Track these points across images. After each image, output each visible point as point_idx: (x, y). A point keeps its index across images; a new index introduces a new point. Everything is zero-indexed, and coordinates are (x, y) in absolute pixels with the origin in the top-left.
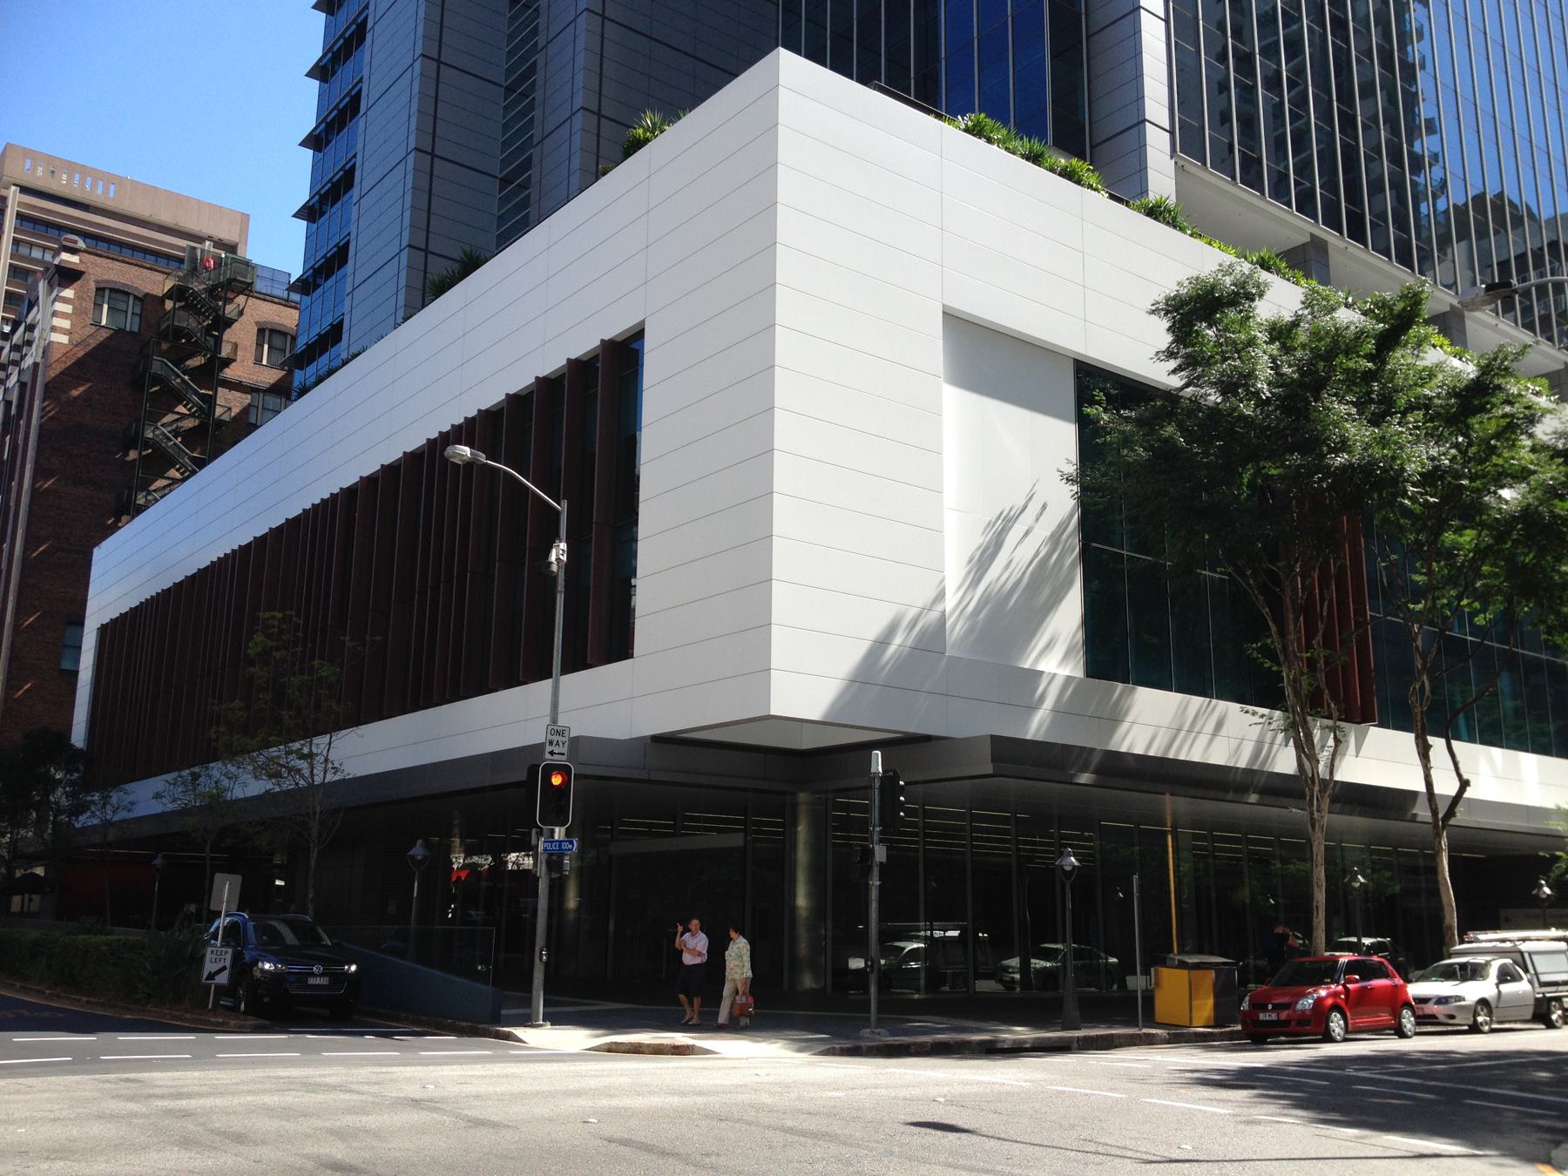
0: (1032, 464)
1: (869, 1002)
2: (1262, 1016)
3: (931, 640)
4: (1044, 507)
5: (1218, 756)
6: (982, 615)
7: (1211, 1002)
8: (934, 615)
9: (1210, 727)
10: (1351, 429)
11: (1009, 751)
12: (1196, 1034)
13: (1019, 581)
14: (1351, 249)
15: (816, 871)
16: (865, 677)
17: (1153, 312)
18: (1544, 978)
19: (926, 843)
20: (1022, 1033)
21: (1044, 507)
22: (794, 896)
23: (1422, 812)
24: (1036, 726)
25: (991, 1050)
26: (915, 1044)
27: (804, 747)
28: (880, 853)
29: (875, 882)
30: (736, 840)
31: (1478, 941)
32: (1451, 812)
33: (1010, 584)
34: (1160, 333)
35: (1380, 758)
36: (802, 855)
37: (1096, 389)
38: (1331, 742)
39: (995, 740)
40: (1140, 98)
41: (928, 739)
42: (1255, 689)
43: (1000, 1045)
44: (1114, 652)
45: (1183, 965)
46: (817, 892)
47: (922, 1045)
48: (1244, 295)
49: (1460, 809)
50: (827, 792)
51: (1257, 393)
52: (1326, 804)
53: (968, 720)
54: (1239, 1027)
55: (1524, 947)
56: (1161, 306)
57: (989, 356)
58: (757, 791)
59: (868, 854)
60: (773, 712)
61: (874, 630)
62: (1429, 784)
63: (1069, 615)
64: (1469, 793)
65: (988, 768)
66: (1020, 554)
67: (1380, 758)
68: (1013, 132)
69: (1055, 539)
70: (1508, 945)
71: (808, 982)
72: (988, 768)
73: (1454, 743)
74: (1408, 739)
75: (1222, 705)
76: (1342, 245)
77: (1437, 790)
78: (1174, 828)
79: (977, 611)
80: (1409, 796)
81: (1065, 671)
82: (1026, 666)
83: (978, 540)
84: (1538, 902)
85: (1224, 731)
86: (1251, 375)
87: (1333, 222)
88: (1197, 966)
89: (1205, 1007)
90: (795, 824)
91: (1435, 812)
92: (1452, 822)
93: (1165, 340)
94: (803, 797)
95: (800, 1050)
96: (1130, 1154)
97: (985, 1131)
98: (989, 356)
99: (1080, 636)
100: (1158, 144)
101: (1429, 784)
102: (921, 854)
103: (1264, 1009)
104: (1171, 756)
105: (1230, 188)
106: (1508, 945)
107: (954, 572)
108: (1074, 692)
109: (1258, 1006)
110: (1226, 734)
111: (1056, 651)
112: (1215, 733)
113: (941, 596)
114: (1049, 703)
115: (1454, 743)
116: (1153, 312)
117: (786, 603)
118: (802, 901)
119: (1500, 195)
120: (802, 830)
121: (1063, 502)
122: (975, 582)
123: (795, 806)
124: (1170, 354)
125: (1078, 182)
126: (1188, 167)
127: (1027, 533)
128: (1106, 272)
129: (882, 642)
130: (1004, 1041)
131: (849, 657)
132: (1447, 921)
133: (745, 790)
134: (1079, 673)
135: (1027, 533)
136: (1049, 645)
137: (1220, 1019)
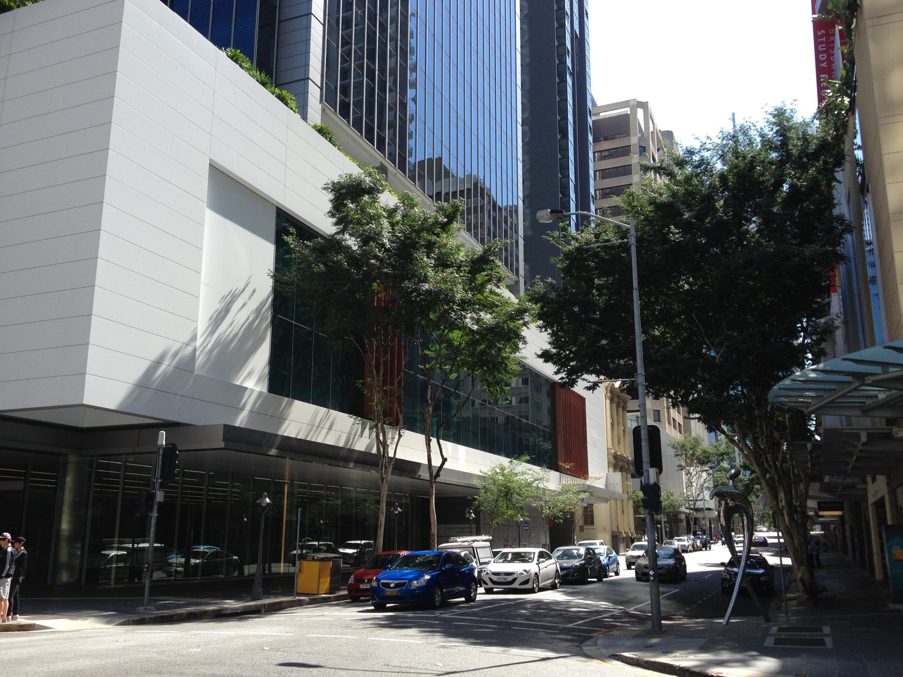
0: (248, 266)
1: (144, 587)
2: (362, 586)
3: (185, 366)
4: (254, 291)
5: (330, 441)
6: (215, 352)
7: (329, 579)
8: (189, 349)
9: (327, 426)
10: (431, 273)
11: (232, 434)
12: (322, 598)
13: (236, 334)
14: (398, 175)
15: (78, 505)
16: (143, 385)
17: (325, 189)
18: (482, 561)
19: (125, 489)
20: (231, 604)
21: (254, 291)
22: (60, 522)
23: (424, 474)
24: (241, 421)
25: (220, 616)
26: (177, 615)
27: (85, 426)
28: (160, 496)
29: (155, 514)
30: (19, 485)
31: (457, 541)
32: (438, 475)
33: (232, 335)
34: (325, 201)
35: (410, 447)
36: (68, 497)
37: (286, 227)
38: (397, 437)
39: (225, 426)
40: (307, 65)
41: (191, 425)
42: (354, 405)
43: (224, 612)
44: (285, 380)
45: (314, 559)
46: (78, 522)
47: (180, 615)
48: (372, 191)
49: (442, 473)
50: (92, 456)
51: (383, 245)
52: (390, 470)
53: (207, 416)
54: (346, 592)
55: (475, 544)
56: (330, 186)
57: (232, 195)
58: (35, 452)
59: (152, 496)
60: (86, 401)
61: (154, 355)
62: (429, 460)
63: (261, 357)
64: (447, 466)
65: (222, 445)
66: (239, 317)
67: (410, 447)
68: (255, 65)
69: (258, 311)
70: (466, 544)
71: (65, 577)
72: (222, 445)
73: (441, 441)
74: (421, 438)
75: (335, 414)
76: (395, 171)
77: (433, 464)
78: (292, 480)
79: (212, 350)
80: (416, 466)
81: (258, 389)
82: (238, 384)
83: (216, 306)
84: (468, 521)
85: (334, 428)
86: (379, 234)
87: (392, 158)
88: (322, 560)
89: (326, 583)
90: (64, 476)
91: (431, 474)
92: (438, 480)
93: (329, 206)
94: (72, 458)
95: (108, 623)
96: (412, 670)
97: (330, 663)
98: (232, 195)
99: (267, 370)
100: (314, 93)
101: (429, 460)
102: (120, 494)
103: (363, 582)
104: (308, 439)
105: (346, 128)
106: (466, 544)
107: (202, 325)
108: (263, 401)
109: (360, 580)
110: (336, 428)
111: (253, 376)
112: (330, 429)
113: (194, 338)
114: (248, 407)
115: (441, 441)
116: (325, 189)
117: (100, 331)
118: (65, 526)
119: (440, 160)
120: (69, 480)
121: (265, 287)
122: (212, 332)
123: (65, 464)
124: (333, 216)
125: (286, 104)
126: (327, 111)
127: (244, 305)
128: (302, 162)
129: (158, 362)
130: (226, 609)
131: (134, 373)
132: (432, 531)
133: (28, 451)
134: (265, 390)
135: (244, 305)
136: (250, 374)
137: (332, 590)
